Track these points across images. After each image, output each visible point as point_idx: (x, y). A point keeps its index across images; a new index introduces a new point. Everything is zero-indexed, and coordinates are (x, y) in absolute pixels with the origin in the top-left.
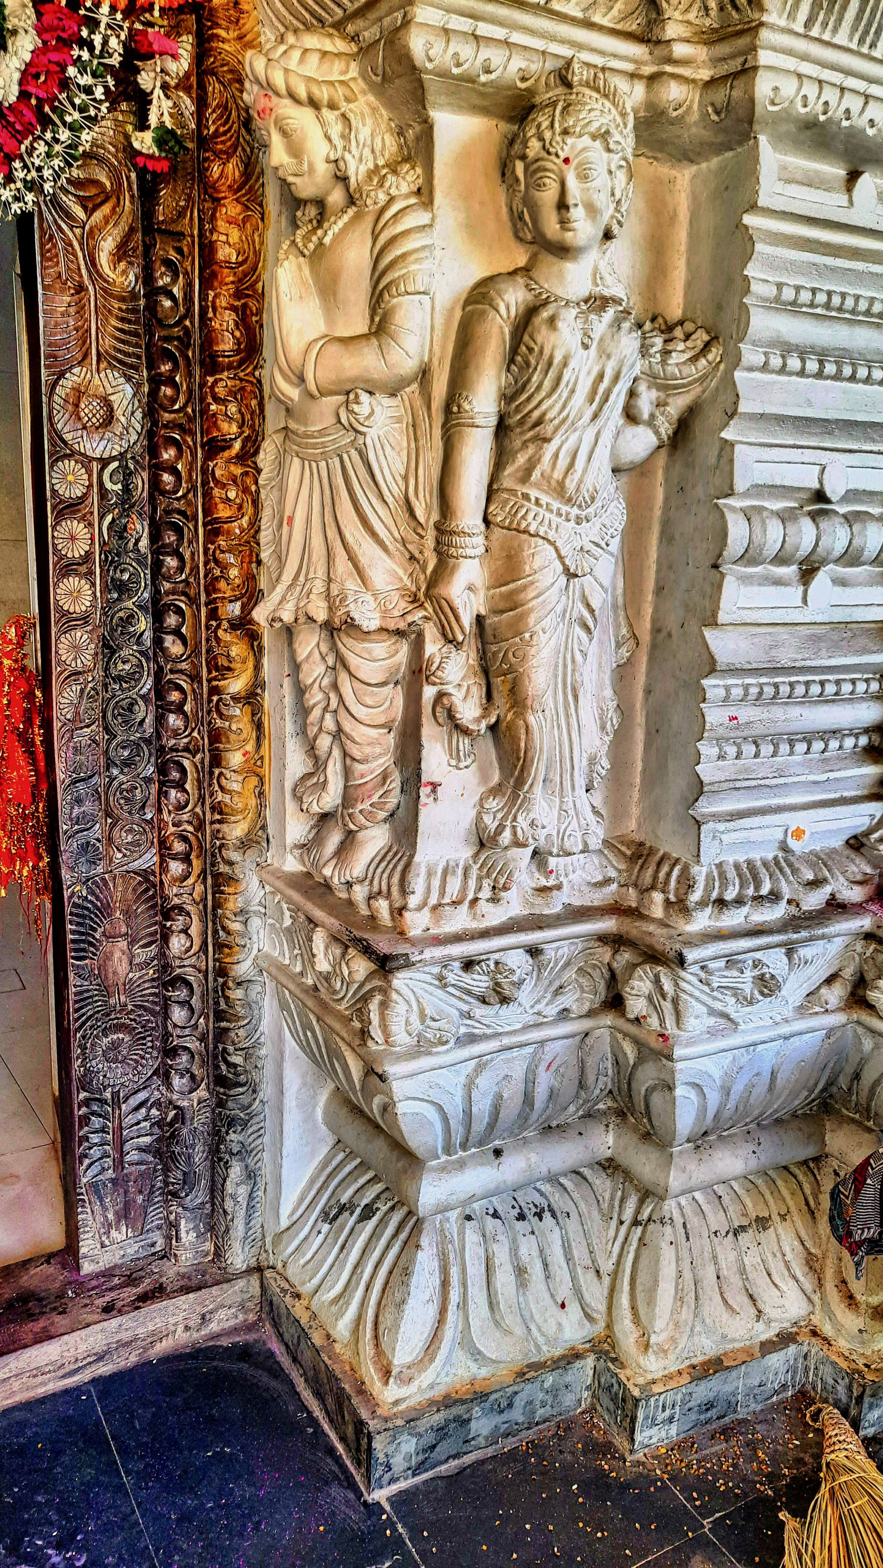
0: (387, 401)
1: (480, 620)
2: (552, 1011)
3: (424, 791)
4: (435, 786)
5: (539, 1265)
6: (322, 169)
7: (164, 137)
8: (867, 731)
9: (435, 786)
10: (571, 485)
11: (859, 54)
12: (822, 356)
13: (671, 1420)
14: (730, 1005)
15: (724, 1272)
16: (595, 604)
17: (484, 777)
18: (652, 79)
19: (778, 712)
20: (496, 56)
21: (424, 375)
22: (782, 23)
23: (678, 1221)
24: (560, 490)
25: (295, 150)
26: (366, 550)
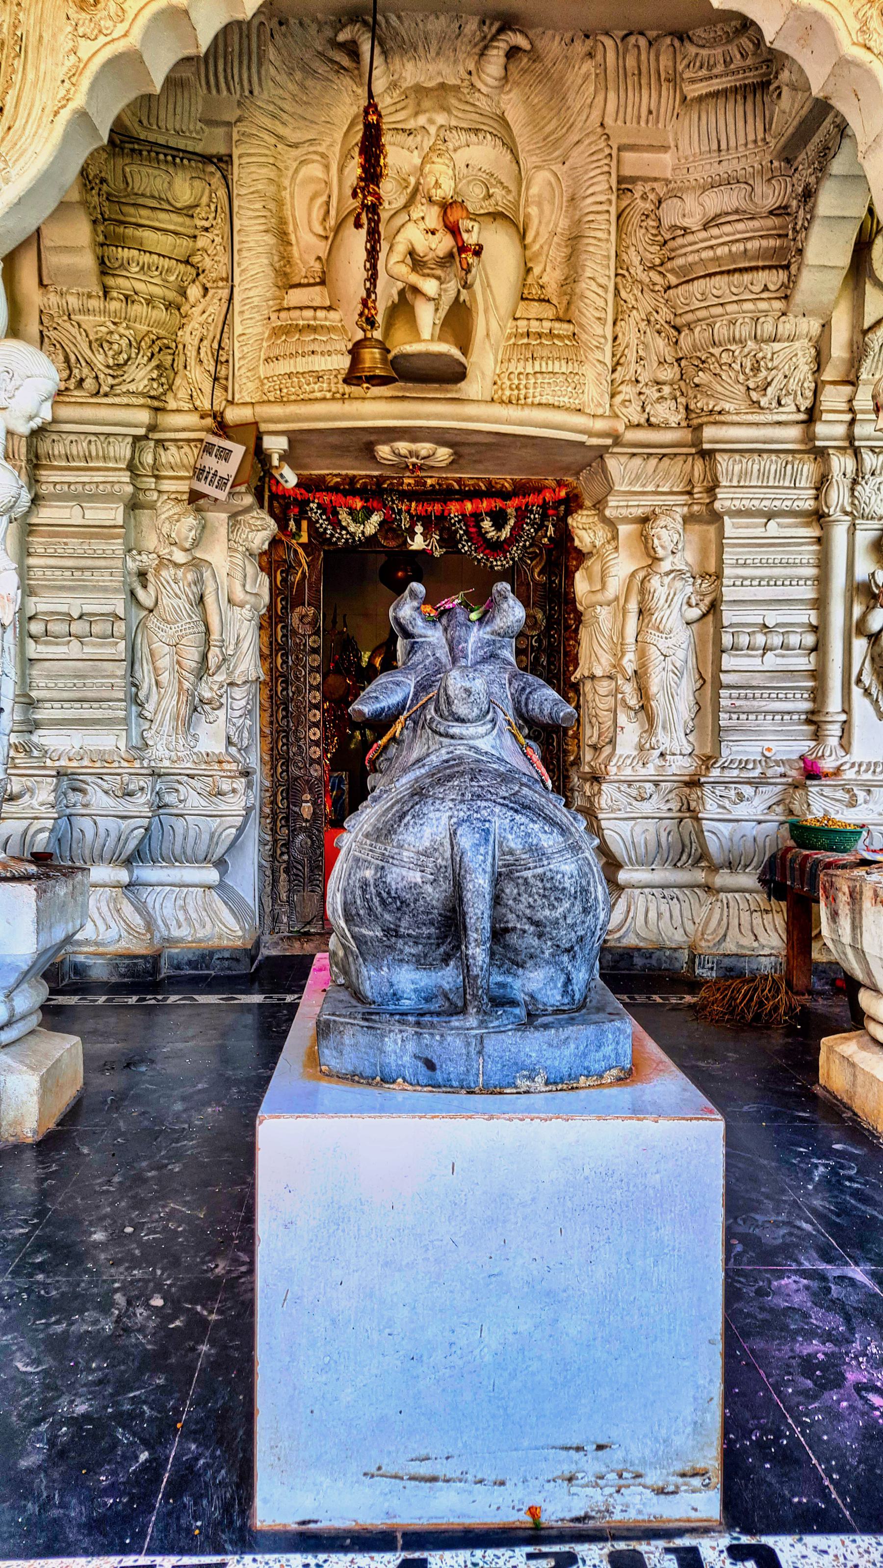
0: (606, 608)
1: (635, 672)
2: (666, 808)
3: (618, 729)
4: (622, 728)
5: (668, 914)
6: (589, 544)
7: (550, 539)
8: (807, 713)
9: (622, 728)
10: (661, 627)
11: (760, 487)
12: (762, 579)
13: (712, 969)
14: (727, 803)
15: (742, 923)
16: (678, 665)
17: (642, 726)
18: (690, 505)
19: (755, 703)
20: (633, 510)
21: (617, 599)
22: (728, 484)
23: (725, 901)
24: (658, 629)
25: (581, 541)
26: (600, 652)
